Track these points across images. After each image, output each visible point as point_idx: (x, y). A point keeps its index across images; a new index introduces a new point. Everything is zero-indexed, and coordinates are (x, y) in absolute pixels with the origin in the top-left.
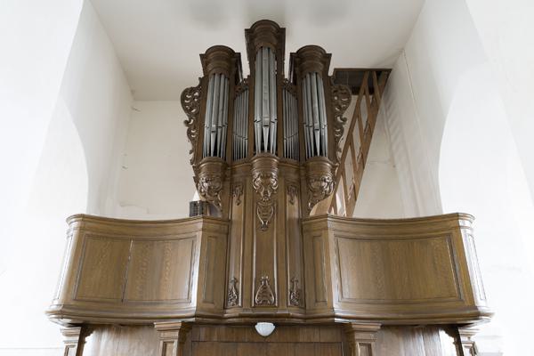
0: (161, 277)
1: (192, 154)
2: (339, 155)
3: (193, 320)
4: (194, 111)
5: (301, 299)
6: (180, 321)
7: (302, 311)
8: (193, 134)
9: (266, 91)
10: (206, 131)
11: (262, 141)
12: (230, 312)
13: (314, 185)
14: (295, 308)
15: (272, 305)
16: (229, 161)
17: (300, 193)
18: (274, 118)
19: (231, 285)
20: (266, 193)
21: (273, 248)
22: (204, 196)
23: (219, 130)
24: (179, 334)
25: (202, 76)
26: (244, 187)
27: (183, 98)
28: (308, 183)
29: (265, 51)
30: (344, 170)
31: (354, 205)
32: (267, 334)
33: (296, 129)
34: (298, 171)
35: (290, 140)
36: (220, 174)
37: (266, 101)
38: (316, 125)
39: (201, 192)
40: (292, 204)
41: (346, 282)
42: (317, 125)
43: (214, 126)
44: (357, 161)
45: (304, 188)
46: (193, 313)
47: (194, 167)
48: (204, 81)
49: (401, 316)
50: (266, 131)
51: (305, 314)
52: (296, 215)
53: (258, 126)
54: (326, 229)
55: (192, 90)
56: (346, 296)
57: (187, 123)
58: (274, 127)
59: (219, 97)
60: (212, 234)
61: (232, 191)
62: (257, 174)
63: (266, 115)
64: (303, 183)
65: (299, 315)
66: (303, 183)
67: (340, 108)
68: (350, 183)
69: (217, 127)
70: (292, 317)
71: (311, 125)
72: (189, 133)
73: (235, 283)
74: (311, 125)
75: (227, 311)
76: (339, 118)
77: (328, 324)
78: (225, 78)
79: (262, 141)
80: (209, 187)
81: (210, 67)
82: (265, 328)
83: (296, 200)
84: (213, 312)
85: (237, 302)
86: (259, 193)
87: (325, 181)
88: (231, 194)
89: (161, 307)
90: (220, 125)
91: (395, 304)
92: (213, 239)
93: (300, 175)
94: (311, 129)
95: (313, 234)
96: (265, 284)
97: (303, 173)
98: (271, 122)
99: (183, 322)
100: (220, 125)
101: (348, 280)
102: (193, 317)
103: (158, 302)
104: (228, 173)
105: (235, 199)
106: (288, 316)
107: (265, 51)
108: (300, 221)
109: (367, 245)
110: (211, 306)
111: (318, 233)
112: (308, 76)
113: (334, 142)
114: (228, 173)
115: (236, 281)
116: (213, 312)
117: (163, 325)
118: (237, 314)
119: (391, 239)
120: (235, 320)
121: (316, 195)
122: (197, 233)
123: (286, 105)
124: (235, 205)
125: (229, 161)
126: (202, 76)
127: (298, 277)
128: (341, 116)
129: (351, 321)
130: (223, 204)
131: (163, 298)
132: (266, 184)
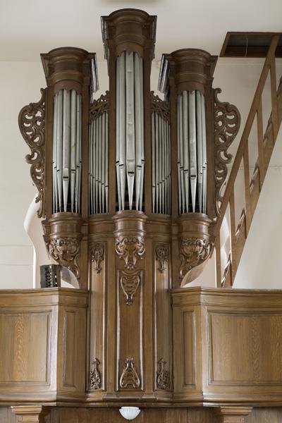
0: (12, 356)
1: (40, 202)
2: (219, 204)
3: (55, 404)
4: (37, 140)
5: (168, 382)
6: (40, 405)
7: (170, 395)
8: (28, 122)
9: (130, 121)
10: (56, 176)
11: (126, 189)
12: (94, 396)
13: (187, 250)
14: (161, 392)
15: (138, 389)
16: (85, 214)
17: (169, 256)
18: (141, 157)
19: (93, 367)
20: (130, 260)
21: (139, 312)
22: (58, 260)
23: (73, 175)
24: (39, 419)
25: (45, 86)
26: (105, 248)
27: (22, 120)
28: (181, 247)
29: (129, 58)
30: (232, 195)
31: (244, 244)
32: (132, 418)
33: (168, 172)
34: (169, 228)
35: (159, 190)
36: (76, 236)
37: (130, 136)
38: (192, 169)
39: (53, 255)
40: (161, 272)
41: (218, 363)
42: (193, 170)
43: (66, 170)
44: (252, 175)
45: (176, 250)
46: (54, 398)
47: (43, 222)
48: (48, 94)
49: (275, 399)
50: (131, 180)
51: (172, 398)
52: (165, 286)
53: (121, 172)
54: (198, 304)
55: (32, 108)
56: (217, 378)
57: (29, 158)
58: (140, 173)
59: (70, 128)
60: (69, 309)
61: (90, 254)
62: (121, 238)
63: (130, 156)
64: (175, 244)
65: (165, 399)
66: (175, 244)
67: (225, 139)
68: (225, 264)
69: (70, 171)
70: (159, 401)
71: (186, 168)
72: (34, 174)
73: (97, 365)
74: (186, 168)
75: (90, 395)
76: (222, 153)
77: (196, 407)
78: (77, 93)
79: (126, 189)
80: (64, 252)
81: (57, 76)
82: (129, 412)
83: (165, 266)
84: (74, 396)
85: (100, 385)
86: (122, 259)
87: (200, 245)
88: (90, 260)
89: (17, 389)
90: (73, 167)
91: (269, 384)
92: (71, 314)
93: (171, 234)
94: (187, 175)
95: (184, 309)
96: (130, 366)
97: (175, 230)
98: (136, 166)
99: (43, 407)
100: (73, 167)
101: (221, 362)
102: (54, 401)
103: (12, 384)
104: (84, 230)
105: (95, 265)
106: (154, 401)
107: (129, 58)
108: (169, 292)
109: (245, 320)
110: (72, 389)
111: (189, 308)
112: (185, 93)
113: (214, 186)
114: (84, 230)
115: (98, 362)
116: (74, 396)
117: (22, 409)
118: (101, 399)
119: (272, 312)
120: (98, 404)
121: (188, 260)
122: (53, 308)
123: (155, 137)
124: (94, 273)
125: (85, 214)
126: (45, 86)
127: (166, 358)
128: (225, 151)
129: (221, 404)
130: (80, 272)
131: (18, 378)
132: (131, 242)
